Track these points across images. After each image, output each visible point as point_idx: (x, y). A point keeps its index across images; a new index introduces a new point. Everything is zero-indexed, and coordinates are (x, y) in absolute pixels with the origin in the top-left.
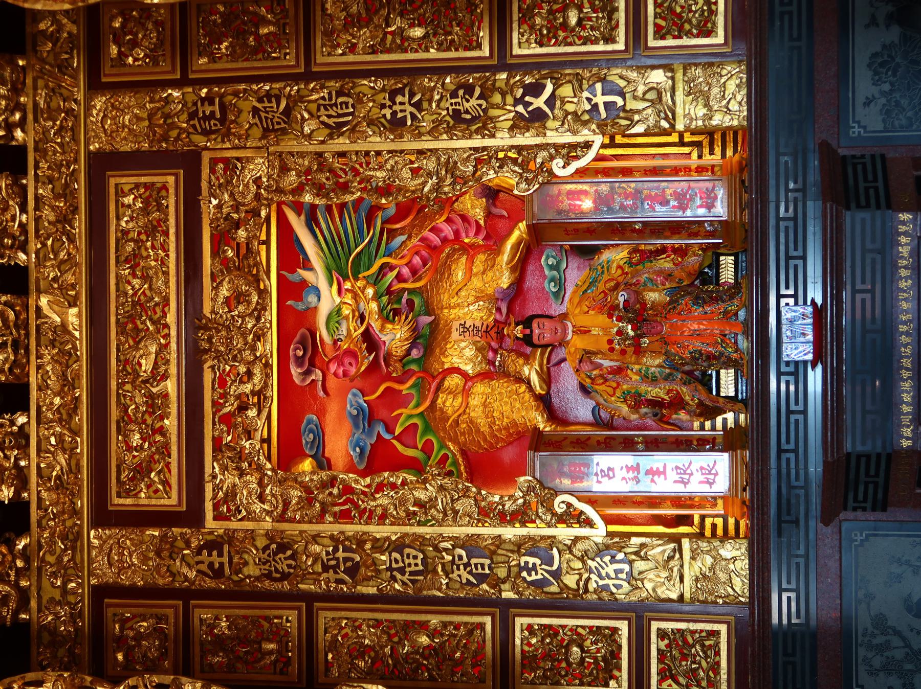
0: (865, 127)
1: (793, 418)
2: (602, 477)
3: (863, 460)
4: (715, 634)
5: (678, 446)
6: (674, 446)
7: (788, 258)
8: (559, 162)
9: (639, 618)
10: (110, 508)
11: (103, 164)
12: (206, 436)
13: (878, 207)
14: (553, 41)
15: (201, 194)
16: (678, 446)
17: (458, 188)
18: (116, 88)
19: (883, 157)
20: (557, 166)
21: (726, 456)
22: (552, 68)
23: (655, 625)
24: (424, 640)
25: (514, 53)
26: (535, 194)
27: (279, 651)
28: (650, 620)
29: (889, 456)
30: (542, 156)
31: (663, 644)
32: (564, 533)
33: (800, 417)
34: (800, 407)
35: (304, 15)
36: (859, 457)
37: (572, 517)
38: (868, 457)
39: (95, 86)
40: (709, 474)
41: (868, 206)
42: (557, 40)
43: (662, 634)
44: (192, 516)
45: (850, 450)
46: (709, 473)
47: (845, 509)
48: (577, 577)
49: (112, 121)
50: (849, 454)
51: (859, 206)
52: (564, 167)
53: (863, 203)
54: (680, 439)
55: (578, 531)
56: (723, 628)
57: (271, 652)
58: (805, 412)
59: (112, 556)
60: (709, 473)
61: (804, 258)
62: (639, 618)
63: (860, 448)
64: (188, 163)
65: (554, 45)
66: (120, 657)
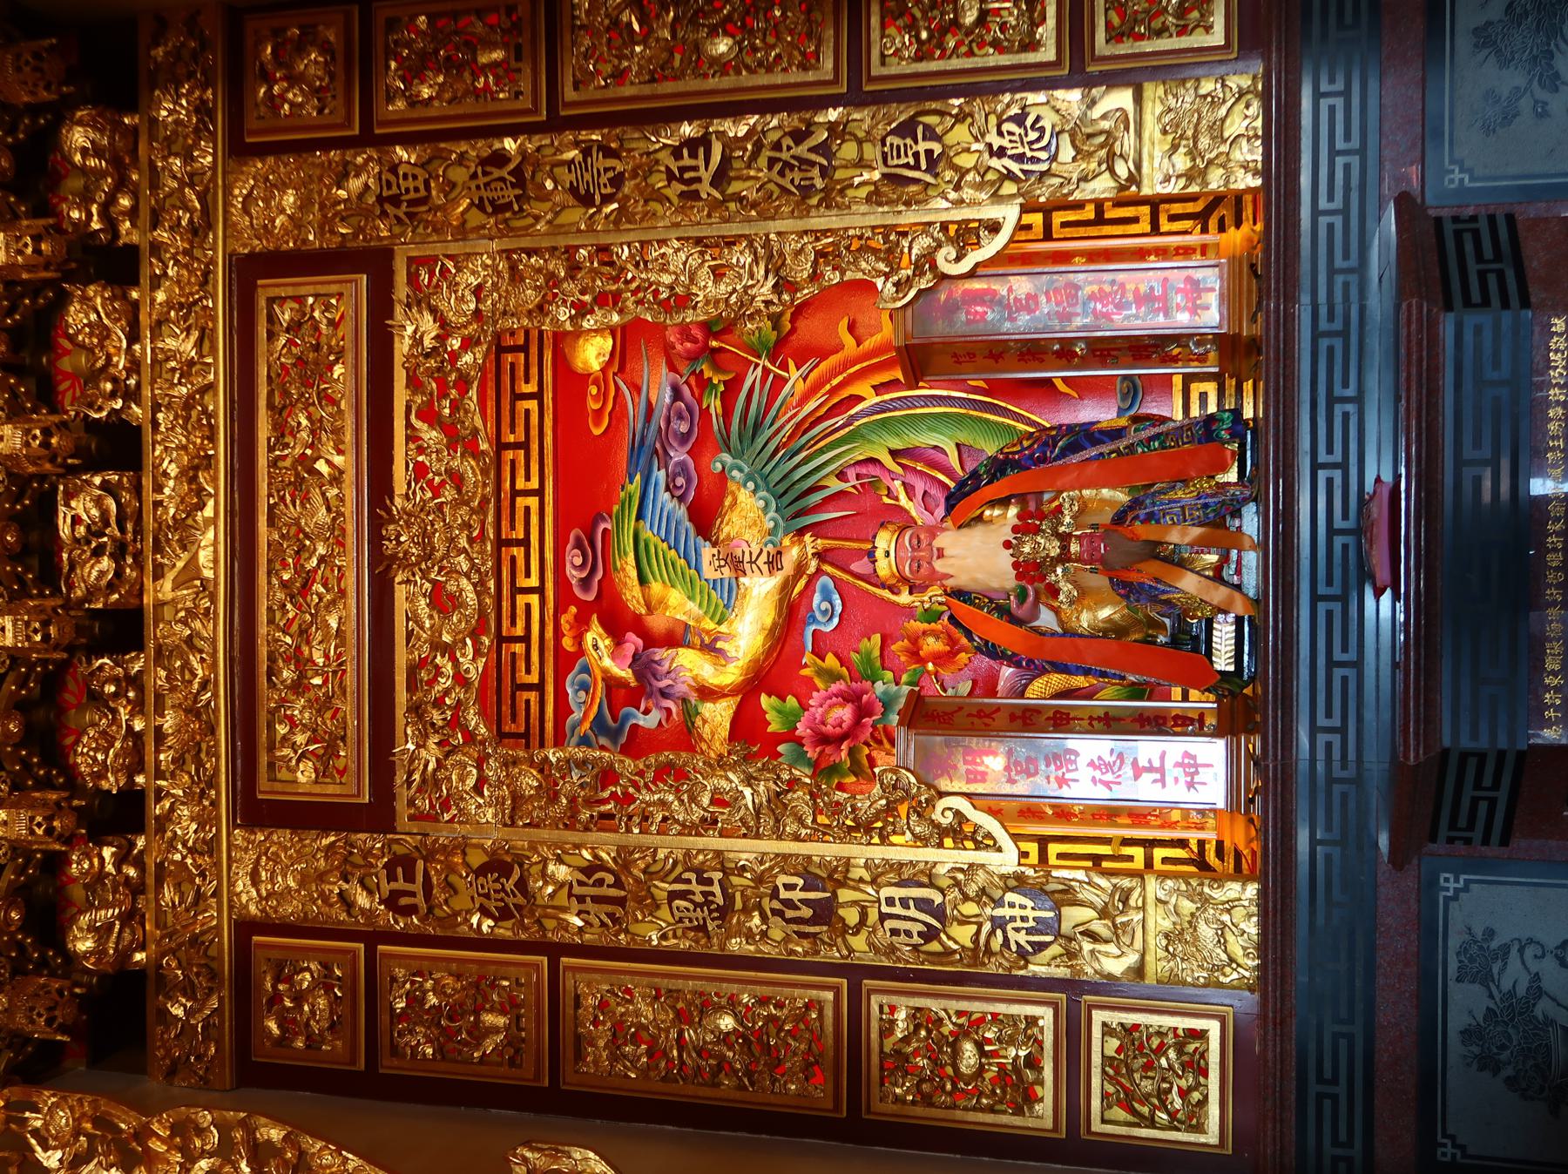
0: (1470, 171)
1: (1338, 673)
2: (1018, 773)
3: (1472, 763)
4: (1200, 1035)
5: (1142, 726)
6: (1137, 726)
7: (1332, 401)
8: (949, 251)
9: (1073, 1006)
10: (260, 797)
11: (250, 271)
12: (397, 688)
13: (1505, 305)
14: (938, 53)
15: (391, 317)
16: (1142, 726)
17: (549, 185)
18: (262, 151)
19: (1510, 219)
20: (945, 260)
21: (1220, 745)
22: (931, 92)
23: (1099, 1017)
24: (727, 1023)
25: (874, 72)
26: (909, 312)
27: (507, 1028)
28: (1090, 1007)
29: (1521, 755)
30: (923, 242)
31: (1114, 1043)
32: (947, 858)
33: (1350, 673)
34: (1352, 655)
35: (542, 24)
36: (1464, 756)
37: (959, 832)
38: (1482, 757)
39: (239, 150)
40: (1192, 773)
41: (1486, 302)
42: (944, 50)
43: (1107, 1030)
44: (379, 815)
45: (1447, 742)
46: (1191, 767)
47: (1433, 838)
48: (974, 928)
49: (273, 206)
50: (1445, 753)
51: (1468, 303)
52: (958, 259)
53: (1476, 296)
54: (1146, 714)
55: (969, 856)
56: (1213, 1027)
57: (495, 1030)
58: (1358, 664)
59: (259, 878)
60: (1191, 767)
61: (1359, 400)
62: (1073, 1006)
63: (1466, 743)
64: (377, 264)
65: (940, 58)
66: (272, 1025)
